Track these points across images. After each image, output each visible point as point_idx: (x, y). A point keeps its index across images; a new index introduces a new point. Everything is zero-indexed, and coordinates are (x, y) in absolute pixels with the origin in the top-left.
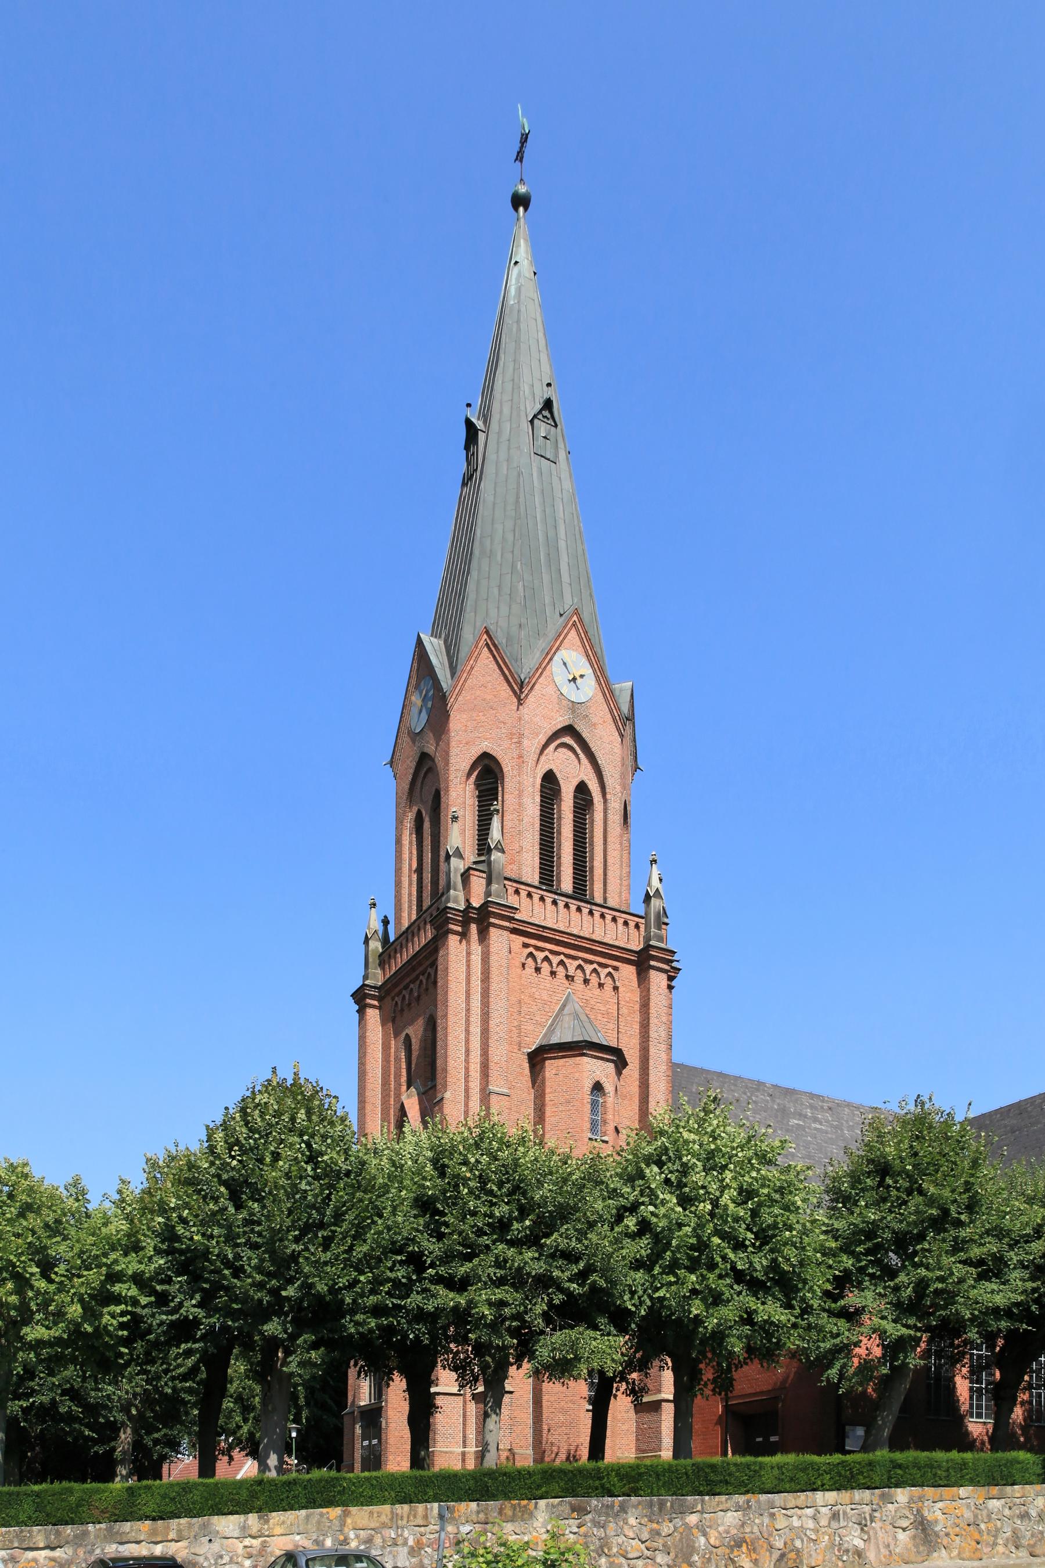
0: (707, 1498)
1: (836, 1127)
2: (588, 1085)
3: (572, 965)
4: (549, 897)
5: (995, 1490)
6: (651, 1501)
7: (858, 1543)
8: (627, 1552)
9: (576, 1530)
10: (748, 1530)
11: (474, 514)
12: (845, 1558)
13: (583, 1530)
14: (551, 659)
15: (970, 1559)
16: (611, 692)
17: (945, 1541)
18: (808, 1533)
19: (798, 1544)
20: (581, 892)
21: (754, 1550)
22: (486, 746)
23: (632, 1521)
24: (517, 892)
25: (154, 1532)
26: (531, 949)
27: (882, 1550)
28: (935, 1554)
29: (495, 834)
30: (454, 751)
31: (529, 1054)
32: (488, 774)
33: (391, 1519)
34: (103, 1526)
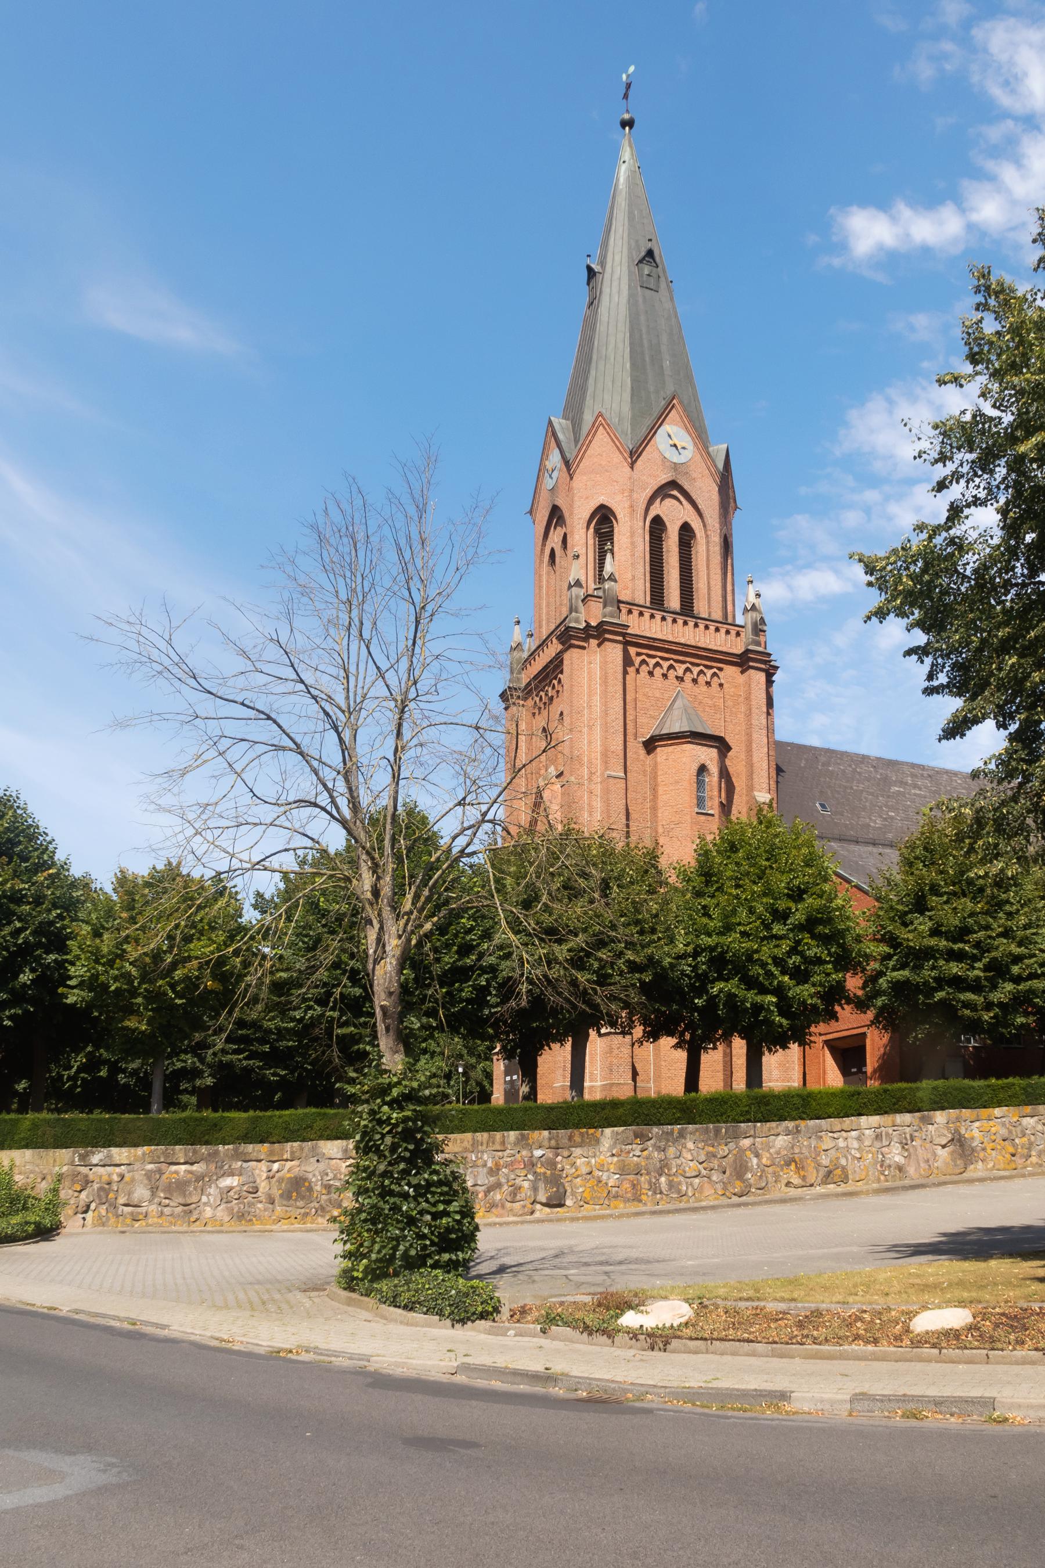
0: (759, 1124)
1: (935, 792)
2: (695, 767)
3: (680, 669)
4: (658, 615)
5: (1028, 1109)
6: (707, 1128)
7: (898, 1159)
8: (685, 1172)
9: (638, 1153)
10: (797, 1151)
11: (593, 329)
12: (886, 1173)
13: (645, 1153)
14: (655, 433)
15: (1005, 1169)
16: (708, 453)
17: (982, 1155)
18: (853, 1152)
19: (843, 1162)
20: (687, 608)
21: (803, 1168)
22: (602, 499)
23: (690, 1145)
24: (630, 612)
25: (271, 1153)
26: (644, 657)
27: (922, 1165)
28: (972, 1167)
29: (609, 567)
30: (577, 503)
31: (644, 743)
32: (603, 520)
33: (473, 1145)
34: (231, 1147)
